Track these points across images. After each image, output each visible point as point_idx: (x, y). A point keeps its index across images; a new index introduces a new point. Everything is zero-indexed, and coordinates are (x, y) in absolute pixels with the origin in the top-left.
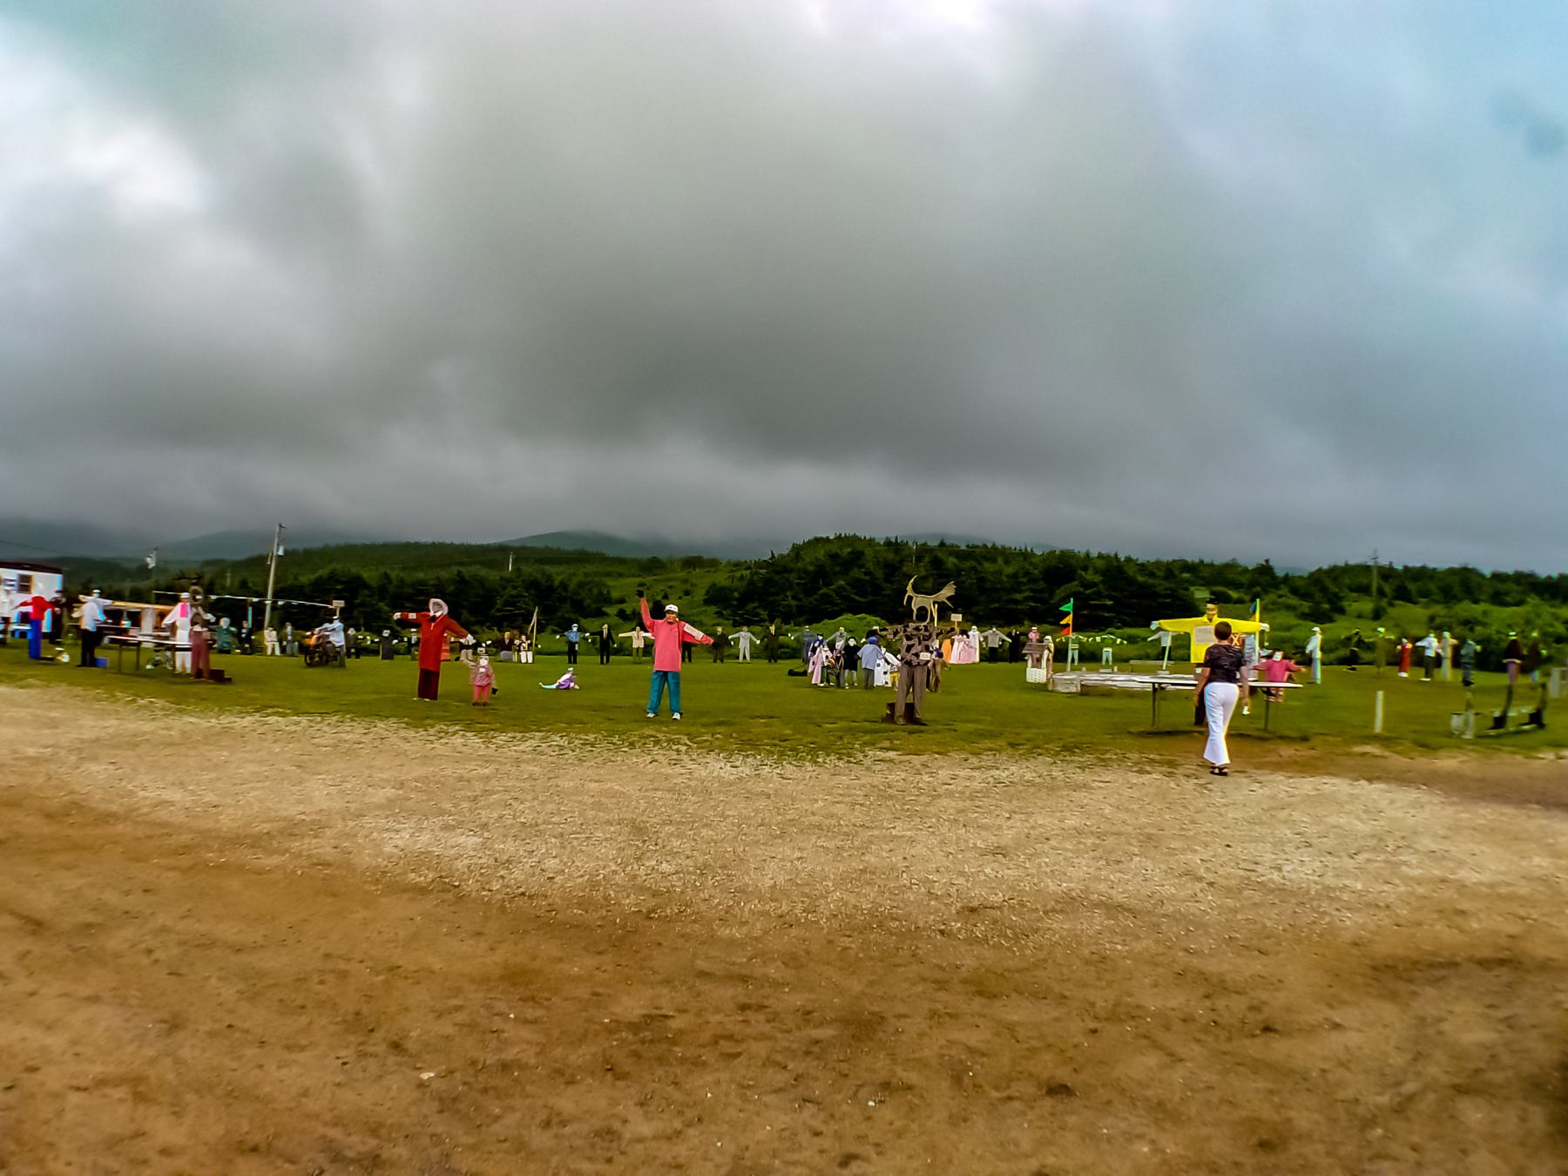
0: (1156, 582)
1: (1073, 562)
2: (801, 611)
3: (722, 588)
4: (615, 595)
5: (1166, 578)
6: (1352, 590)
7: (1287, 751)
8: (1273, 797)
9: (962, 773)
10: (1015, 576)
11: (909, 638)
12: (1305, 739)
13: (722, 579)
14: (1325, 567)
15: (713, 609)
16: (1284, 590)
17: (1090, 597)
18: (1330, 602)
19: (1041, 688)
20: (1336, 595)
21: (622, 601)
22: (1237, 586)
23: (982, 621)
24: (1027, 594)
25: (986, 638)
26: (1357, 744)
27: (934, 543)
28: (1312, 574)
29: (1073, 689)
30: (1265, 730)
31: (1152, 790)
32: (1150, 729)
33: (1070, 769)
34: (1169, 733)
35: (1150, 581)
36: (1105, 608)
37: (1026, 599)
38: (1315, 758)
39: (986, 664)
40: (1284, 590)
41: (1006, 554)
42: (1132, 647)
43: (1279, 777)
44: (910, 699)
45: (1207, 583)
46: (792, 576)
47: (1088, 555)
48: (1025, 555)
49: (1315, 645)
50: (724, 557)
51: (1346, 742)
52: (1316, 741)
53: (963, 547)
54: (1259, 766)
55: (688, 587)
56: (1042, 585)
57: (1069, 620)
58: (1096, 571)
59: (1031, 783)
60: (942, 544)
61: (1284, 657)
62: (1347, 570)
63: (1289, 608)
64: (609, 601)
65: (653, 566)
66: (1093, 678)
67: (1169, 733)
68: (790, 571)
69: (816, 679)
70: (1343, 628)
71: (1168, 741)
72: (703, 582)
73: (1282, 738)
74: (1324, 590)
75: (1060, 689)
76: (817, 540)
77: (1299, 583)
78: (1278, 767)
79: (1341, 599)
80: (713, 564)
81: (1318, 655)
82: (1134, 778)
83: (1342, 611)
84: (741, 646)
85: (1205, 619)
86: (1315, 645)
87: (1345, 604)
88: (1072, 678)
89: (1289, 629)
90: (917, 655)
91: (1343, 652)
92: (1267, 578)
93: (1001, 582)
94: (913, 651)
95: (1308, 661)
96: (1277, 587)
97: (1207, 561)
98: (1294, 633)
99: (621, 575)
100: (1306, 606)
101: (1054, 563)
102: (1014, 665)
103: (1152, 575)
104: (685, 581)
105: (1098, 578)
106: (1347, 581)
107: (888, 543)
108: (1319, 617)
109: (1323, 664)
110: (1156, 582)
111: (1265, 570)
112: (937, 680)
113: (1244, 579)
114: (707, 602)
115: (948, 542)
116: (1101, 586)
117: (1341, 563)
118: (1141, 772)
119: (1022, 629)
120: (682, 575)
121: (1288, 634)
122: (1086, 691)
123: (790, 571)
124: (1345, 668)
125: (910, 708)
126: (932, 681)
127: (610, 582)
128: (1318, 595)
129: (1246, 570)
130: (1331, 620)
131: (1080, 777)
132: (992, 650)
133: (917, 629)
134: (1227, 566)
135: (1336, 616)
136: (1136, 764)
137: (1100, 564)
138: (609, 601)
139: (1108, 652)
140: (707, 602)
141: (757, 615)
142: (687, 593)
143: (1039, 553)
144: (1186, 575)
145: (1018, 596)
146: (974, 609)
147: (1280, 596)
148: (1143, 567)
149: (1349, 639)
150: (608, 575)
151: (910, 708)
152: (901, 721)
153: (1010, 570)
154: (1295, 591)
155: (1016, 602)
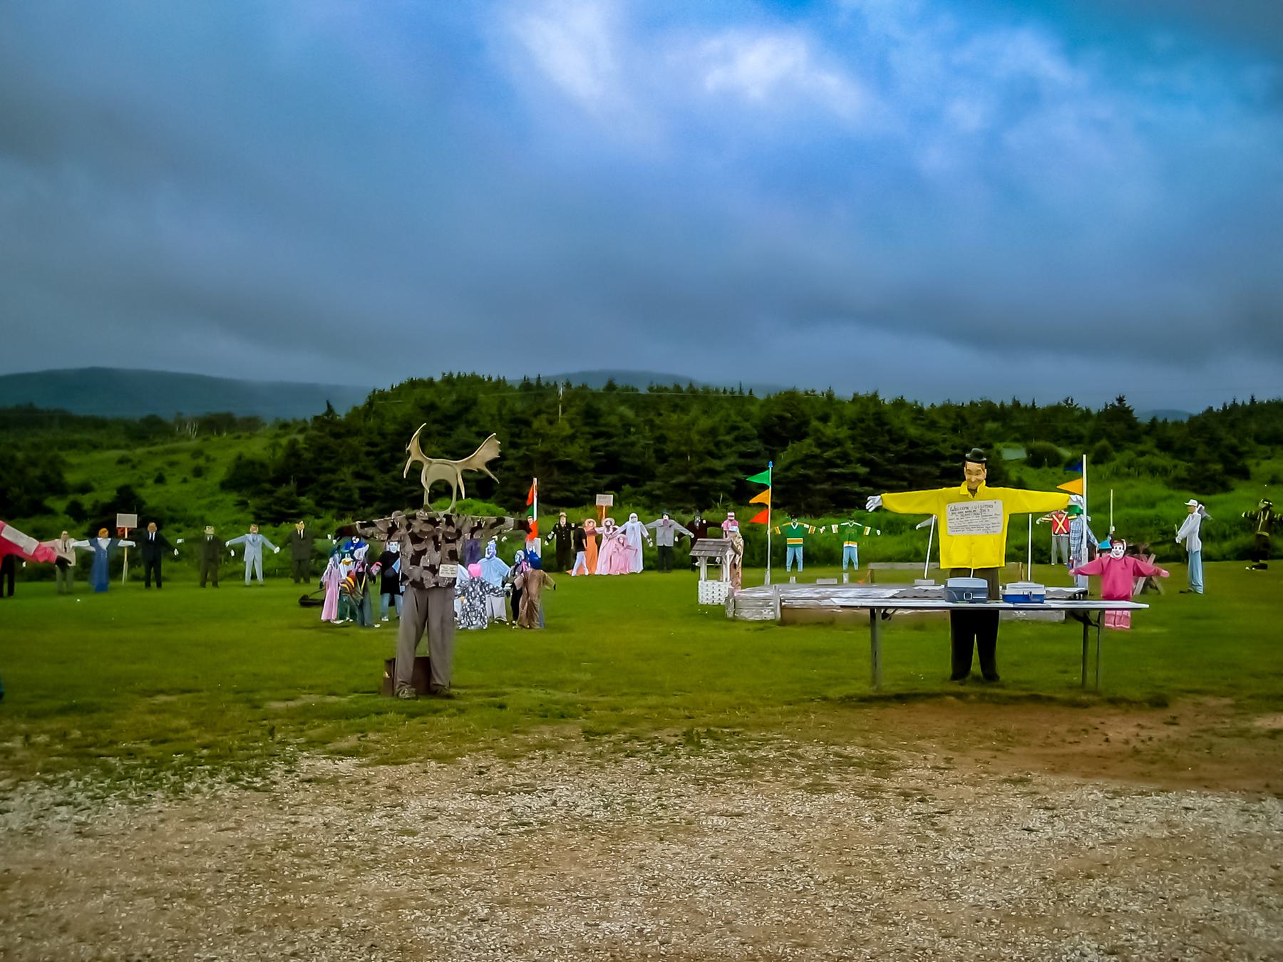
0: (938, 436)
1: (807, 409)
2: (368, 497)
3: (251, 463)
4: (72, 478)
5: (955, 430)
6: (1259, 440)
7: (1120, 730)
8: (1072, 847)
9: (451, 805)
10: (713, 432)
11: (416, 539)
12: (1159, 703)
13: (256, 448)
14: (1218, 407)
15: (232, 497)
16: (1149, 444)
17: (830, 463)
18: (1223, 459)
19: (716, 613)
20: (1233, 449)
21: (85, 489)
22: (1072, 440)
23: (652, 506)
24: (732, 460)
25: (653, 533)
26: (1260, 712)
27: (598, 386)
28: (1193, 419)
29: (768, 615)
30: (1082, 686)
31: (822, 833)
32: (865, 689)
33: (673, 783)
34: (900, 698)
35: (930, 435)
36: (854, 477)
37: (730, 468)
38: (1176, 744)
39: (655, 575)
40: (1149, 444)
41: (706, 398)
42: (895, 539)
43: (1093, 793)
44: (423, 651)
45: (1024, 437)
46: (354, 441)
47: (830, 397)
48: (739, 399)
49: (1190, 530)
50: (269, 415)
51: (1240, 709)
52: (1183, 706)
53: (643, 390)
54: (1059, 766)
55: (201, 462)
56: (757, 445)
57: (765, 497)
58: (841, 422)
59: (586, 825)
60: (611, 387)
61: (1132, 551)
62: (1254, 410)
63: (1153, 470)
64: (60, 489)
65: (149, 430)
66: (802, 593)
67: (900, 698)
68: (357, 433)
69: (329, 612)
70: (1244, 501)
71: (894, 713)
72: (224, 453)
73: (1114, 702)
74: (1213, 442)
75: (747, 614)
76: (413, 384)
77: (1171, 433)
78: (1099, 765)
79: (1240, 455)
80: (251, 425)
81: (1196, 545)
82: (796, 805)
83: (1245, 474)
84: (248, 557)
85: (963, 489)
86: (1190, 530)
87: (1250, 463)
88: (766, 597)
89: (1152, 505)
90: (433, 569)
91: (1244, 540)
92: (1120, 426)
93: (688, 442)
94: (425, 561)
95: (1180, 556)
96: (1136, 439)
97: (1025, 401)
98: (1164, 510)
99: (95, 447)
100: (1182, 468)
101: (777, 411)
102: (759, 570)
103: (932, 425)
104: (197, 454)
105: (844, 433)
106: (1253, 426)
107: (526, 385)
108: (1203, 485)
109: (1207, 558)
110: (938, 436)
111: (1119, 413)
112: (532, 607)
113: (1085, 429)
114: (226, 486)
115: (619, 383)
116: (849, 445)
117: (1243, 399)
118: (813, 789)
119: (708, 515)
120: (194, 443)
121: (1151, 512)
122: (789, 617)
123: (357, 433)
124: (1247, 566)
125: (424, 665)
126: (523, 611)
127: (72, 458)
128: (1201, 451)
129: (1087, 415)
130: (1226, 488)
131: (693, 803)
132: (663, 549)
133: (432, 521)
134: (1056, 411)
135: (1234, 482)
136: (810, 770)
137: (851, 412)
138: (60, 489)
139: (851, 548)
140: (226, 486)
141: (293, 505)
142: (198, 472)
143: (760, 396)
144: (990, 425)
145: (717, 465)
146: (648, 486)
147: (1142, 454)
148: (918, 414)
149: (1253, 518)
150: (73, 445)
151: (424, 665)
152: (406, 692)
153: (705, 423)
154: (1165, 446)
155: (713, 473)
